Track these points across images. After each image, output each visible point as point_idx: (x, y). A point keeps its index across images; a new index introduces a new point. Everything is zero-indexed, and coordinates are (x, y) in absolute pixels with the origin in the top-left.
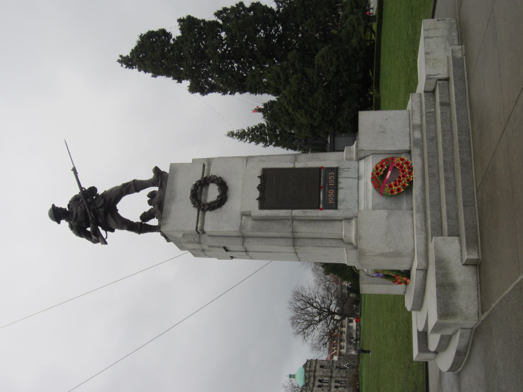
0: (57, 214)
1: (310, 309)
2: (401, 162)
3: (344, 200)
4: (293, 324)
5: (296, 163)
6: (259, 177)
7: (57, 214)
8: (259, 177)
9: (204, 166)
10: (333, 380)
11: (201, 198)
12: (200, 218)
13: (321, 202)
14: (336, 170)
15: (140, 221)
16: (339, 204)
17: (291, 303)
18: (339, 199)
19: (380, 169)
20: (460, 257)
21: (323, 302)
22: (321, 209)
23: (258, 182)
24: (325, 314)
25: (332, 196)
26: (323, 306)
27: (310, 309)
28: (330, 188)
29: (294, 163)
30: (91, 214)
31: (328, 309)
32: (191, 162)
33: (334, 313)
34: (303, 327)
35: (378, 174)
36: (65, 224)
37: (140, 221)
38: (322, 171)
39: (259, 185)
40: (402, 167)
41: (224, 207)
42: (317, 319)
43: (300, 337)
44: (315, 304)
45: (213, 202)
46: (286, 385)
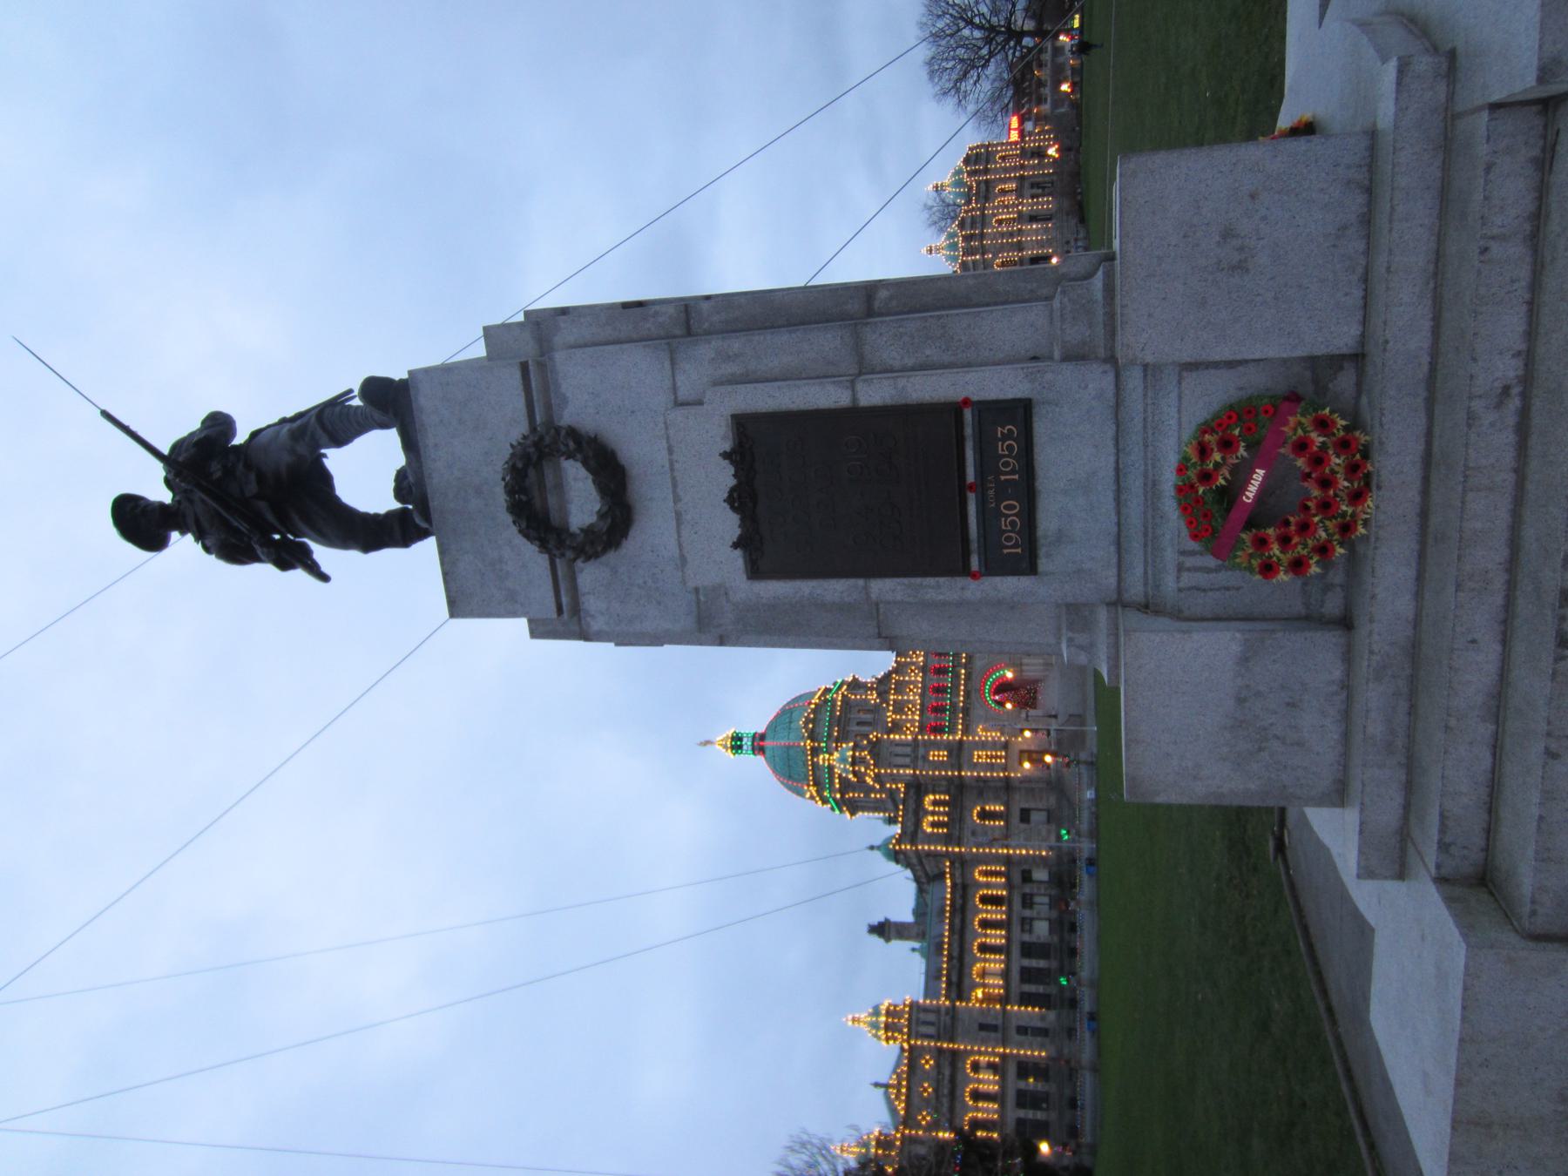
0: (140, 523)
1: (966, 32)
2: (1318, 439)
3: (1060, 537)
4: (932, 74)
5: (859, 386)
6: (725, 455)
7: (140, 523)
8: (725, 455)
9: (524, 368)
10: (1027, 184)
11: (544, 500)
12: (560, 573)
13: (974, 546)
14: (1020, 412)
15: (397, 505)
16: (1042, 552)
17: (922, 25)
18: (1040, 533)
19: (1217, 457)
20: (1427, 324)
21: (995, 11)
22: (975, 576)
23: (725, 477)
24: (1000, 39)
25: (1013, 523)
26: (994, 20)
27: (966, 32)
28: (1003, 491)
29: (853, 383)
30: (243, 495)
31: (1008, 28)
32: (479, 351)
33: (1023, 34)
34: (954, 77)
35: (1206, 477)
36: (183, 545)
37: (397, 505)
38: (968, 414)
39: (732, 490)
40: (1318, 460)
41: (630, 545)
42: (984, 52)
43: (951, 102)
44: (977, 20)
45: (588, 531)
46: (930, 203)
